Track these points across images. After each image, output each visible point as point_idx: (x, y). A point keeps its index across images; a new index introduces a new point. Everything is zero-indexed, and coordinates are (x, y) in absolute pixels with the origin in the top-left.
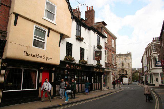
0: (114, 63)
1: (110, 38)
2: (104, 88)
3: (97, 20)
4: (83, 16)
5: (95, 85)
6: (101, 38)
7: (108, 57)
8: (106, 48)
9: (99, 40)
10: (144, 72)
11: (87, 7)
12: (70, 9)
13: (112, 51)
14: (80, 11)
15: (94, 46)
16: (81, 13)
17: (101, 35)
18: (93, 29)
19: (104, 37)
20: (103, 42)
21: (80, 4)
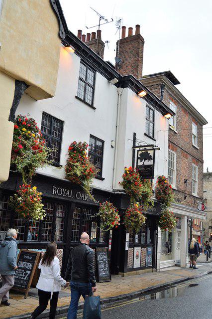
0: (196, 191)
1: (187, 118)
2: (163, 263)
3: (151, 66)
4: (110, 55)
5: (136, 256)
6: (158, 114)
7: (177, 174)
8: (172, 145)
9: (151, 119)
10: (81, 211)
11: (124, 28)
12: (55, 6)
13: (190, 158)
14: (103, 39)
15: (135, 134)
16: (106, 44)
17: (155, 103)
18: (133, 83)
19: (165, 111)
20: (163, 123)
21: (103, 21)
